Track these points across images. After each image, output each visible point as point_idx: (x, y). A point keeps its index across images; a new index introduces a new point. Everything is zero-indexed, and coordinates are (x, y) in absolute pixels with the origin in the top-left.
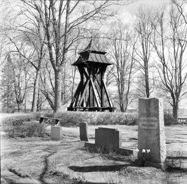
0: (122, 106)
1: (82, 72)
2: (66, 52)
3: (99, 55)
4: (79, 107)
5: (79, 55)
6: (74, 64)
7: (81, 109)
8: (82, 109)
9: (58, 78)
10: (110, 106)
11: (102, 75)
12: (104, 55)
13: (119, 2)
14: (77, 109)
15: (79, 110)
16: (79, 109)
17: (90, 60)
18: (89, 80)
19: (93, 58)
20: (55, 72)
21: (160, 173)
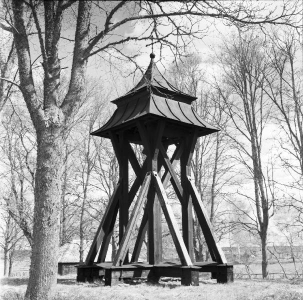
0: (198, 250)
1: (124, 156)
2: (82, 63)
3: (177, 102)
4: (118, 264)
5: (115, 107)
6: (102, 133)
7: (125, 275)
8: (130, 274)
9: (79, 29)
10: (220, 261)
11: (186, 164)
12: (189, 106)
13: (201, 6)
14: (113, 275)
15: (120, 279)
16: (118, 274)
17: (153, 110)
18: (148, 178)
19: (159, 106)
20: (45, 98)
21: (33, 213)
